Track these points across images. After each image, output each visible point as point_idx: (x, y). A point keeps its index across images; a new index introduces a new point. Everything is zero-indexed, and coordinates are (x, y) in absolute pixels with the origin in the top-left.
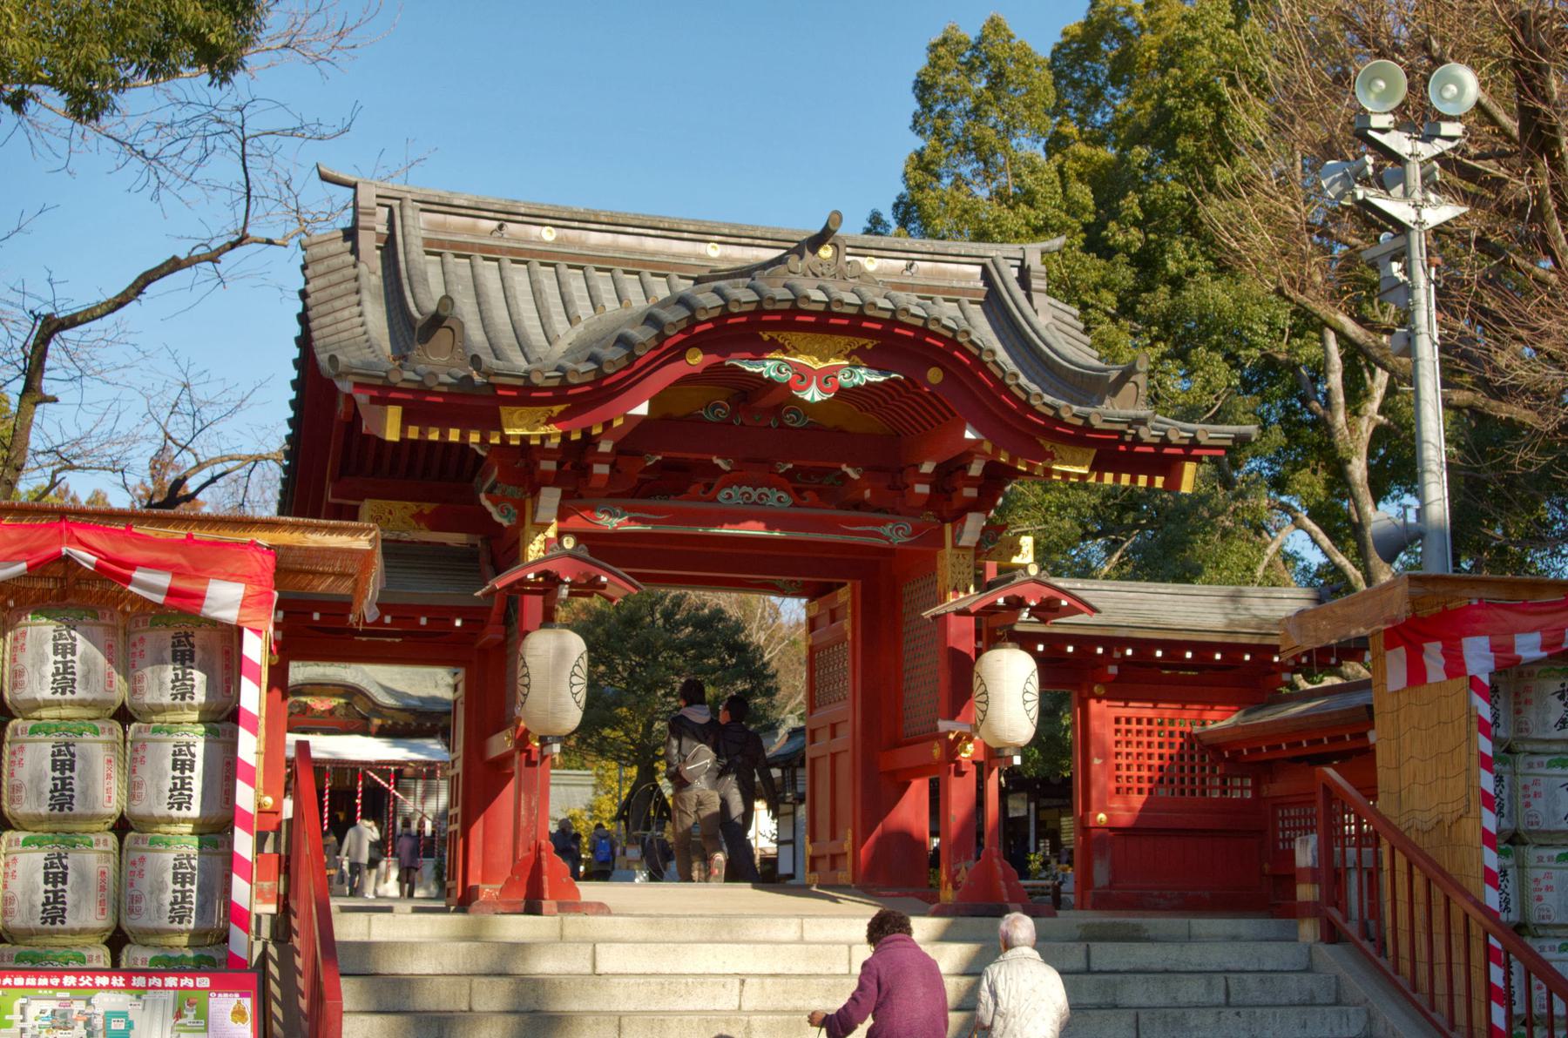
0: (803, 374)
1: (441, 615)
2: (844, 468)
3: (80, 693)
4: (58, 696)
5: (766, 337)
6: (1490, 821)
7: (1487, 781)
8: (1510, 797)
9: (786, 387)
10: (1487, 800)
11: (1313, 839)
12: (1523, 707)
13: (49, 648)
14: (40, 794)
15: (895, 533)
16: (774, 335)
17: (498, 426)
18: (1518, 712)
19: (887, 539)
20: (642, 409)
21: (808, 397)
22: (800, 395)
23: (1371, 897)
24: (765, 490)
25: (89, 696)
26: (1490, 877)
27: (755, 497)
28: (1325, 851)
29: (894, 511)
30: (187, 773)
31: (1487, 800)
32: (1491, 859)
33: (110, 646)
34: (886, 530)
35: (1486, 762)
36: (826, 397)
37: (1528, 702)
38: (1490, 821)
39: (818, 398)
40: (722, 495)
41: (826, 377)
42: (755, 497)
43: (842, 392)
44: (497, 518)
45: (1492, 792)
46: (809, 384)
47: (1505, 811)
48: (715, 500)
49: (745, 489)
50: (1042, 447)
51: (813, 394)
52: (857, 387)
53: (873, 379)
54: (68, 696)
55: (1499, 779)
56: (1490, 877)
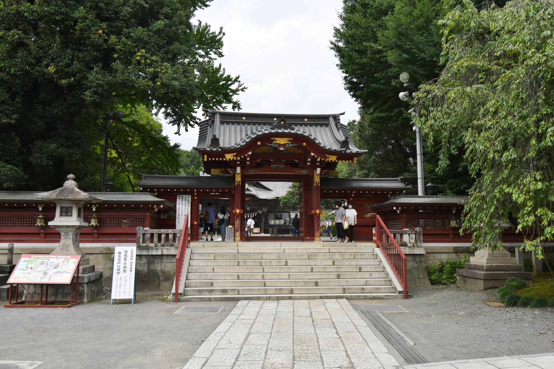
0: (280, 145)
15: (305, 172)
34: (303, 171)
41: (284, 145)
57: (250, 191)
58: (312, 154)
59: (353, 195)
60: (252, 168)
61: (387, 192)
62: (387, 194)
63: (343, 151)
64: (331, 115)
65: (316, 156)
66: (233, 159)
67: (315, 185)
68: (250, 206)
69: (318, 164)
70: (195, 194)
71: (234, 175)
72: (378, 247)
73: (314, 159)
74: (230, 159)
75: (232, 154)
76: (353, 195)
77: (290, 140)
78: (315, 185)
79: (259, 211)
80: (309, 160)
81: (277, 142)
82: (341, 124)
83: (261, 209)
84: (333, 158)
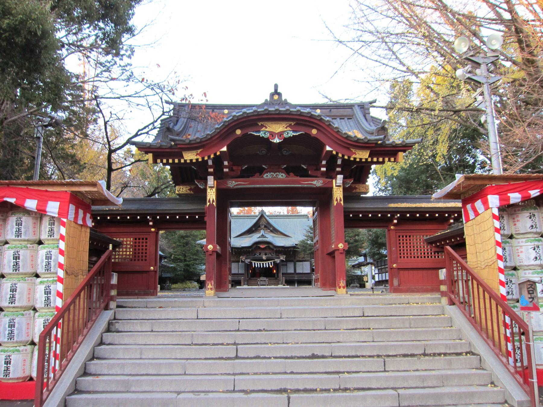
0: (273, 134)
1: (192, 215)
2: (303, 166)
3: (23, 237)
4: (17, 238)
5: (260, 124)
6: (501, 264)
7: (500, 251)
8: (510, 255)
9: (268, 139)
10: (500, 257)
11: (444, 270)
12: (516, 223)
13: (15, 224)
14: (10, 267)
15: (318, 183)
16: (262, 123)
17: (183, 157)
18: (515, 225)
19: (315, 185)
20: (225, 149)
21: (275, 141)
22: (272, 141)
23: (44, 355)
24: (278, 173)
25: (27, 238)
26: (502, 283)
27: (275, 175)
28: (450, 274)
29: (316, 177)
30: (18, 260)
31: (500, 257)
32: (502, 277)
33: (35, 223)
34: (314, 183)
35: (498, 244)
36: (281, 141)
37: (518, 221)
38: (501, 264)
39: (278, 141)
40: (265, 176)
41: (280, 134)
42: (275, 175)
43: (285, 139)
44: (199, 186)
45: (501, 254)
46: (275, 138)
47: (508, 260)
48: (263, 177)
49: (272, 173)
50: (352, 151)
51: (277, 140)
52: (290, 137)
53: (294, 134)
54: (20, 238)
55: (504, 249)
56: (502, 283)
57: (265, 237)
58: (328, 148)
59: (395, 221)
60: (233, 177)
61: (449, 216)
62: (449, 218)
63: (380, 140)
64: (356, 104)
65: (334, 153)
66: (197, 160)
67: (335, 203)
68: (266, 254)
69: (338, 169)
70: (151, 223)
71: (205, 190)
72: (452, 303)
73: (332, 158)
74: (191, 160)
75: (194, 152)
76: (395, 221)
77: (290, 126)
78: (335, 203)
79: (276, 260)
80: (324, 162)
81: (268, 129)
82: (372, 117)
83: (279, 258)
84: (363, 155)
